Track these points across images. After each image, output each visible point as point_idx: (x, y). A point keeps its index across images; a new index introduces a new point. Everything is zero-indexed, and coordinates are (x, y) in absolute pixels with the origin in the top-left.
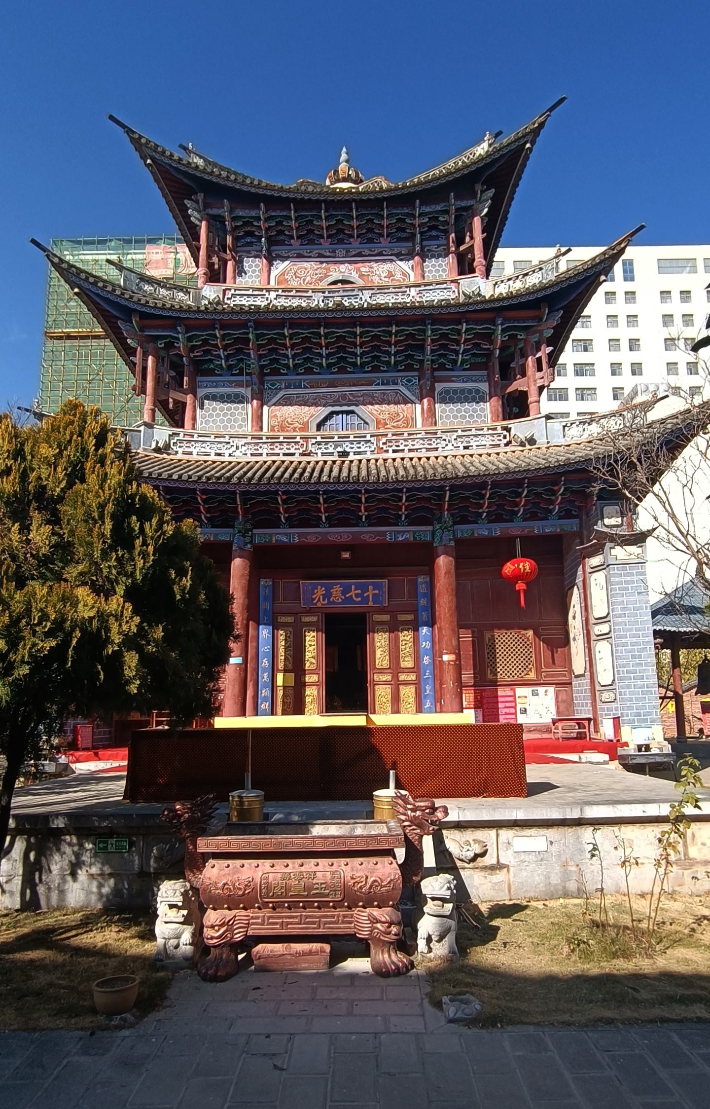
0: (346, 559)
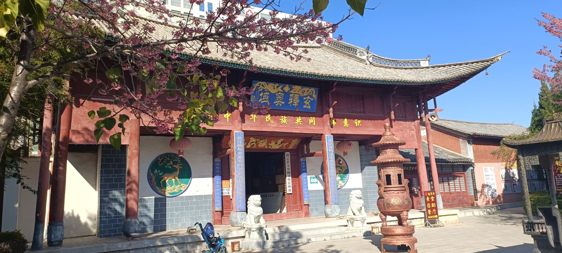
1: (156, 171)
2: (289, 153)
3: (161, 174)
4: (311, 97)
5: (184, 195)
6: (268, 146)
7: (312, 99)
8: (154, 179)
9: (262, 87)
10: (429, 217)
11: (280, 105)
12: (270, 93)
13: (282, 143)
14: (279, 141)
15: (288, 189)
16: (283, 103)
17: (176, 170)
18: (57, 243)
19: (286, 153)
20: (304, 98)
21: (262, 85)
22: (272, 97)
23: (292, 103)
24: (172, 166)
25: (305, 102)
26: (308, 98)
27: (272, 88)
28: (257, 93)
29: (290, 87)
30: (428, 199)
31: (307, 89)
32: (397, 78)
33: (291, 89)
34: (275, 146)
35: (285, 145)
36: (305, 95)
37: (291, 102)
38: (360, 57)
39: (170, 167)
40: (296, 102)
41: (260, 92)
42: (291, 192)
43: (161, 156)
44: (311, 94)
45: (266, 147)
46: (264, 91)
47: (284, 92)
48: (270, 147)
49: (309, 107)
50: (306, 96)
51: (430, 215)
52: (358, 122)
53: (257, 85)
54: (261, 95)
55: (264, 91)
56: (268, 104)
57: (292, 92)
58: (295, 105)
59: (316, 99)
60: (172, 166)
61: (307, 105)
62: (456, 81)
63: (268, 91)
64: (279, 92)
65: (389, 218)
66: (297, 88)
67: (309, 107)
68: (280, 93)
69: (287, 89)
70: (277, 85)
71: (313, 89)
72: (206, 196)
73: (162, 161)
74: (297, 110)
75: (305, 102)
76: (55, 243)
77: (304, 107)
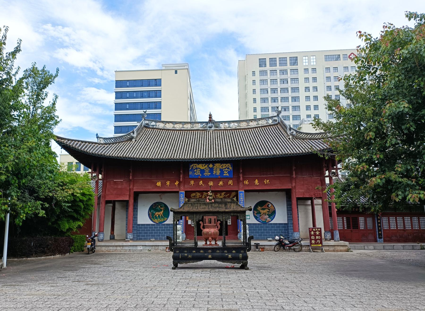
0: (178, 250)
1: (152, 211)
4: (228, 168)
8: (151, 215)
10: (312, 245)
13: (225, 194)
14: (223, 194)
16: (210, 174)
17: (161, 210)
22: (202, 171)
23: (216, 173)
25: (225, 172)
26: (226, 169)
27: (201, 166)
29: (213, 165)
30: (312, 233)
31: (225, 164)
33: (214, 166)
36: (224, 168)
40: (218, 172)
41: (195, 169)
43: (154, 204)
44: (228, 167)
46: (196, 169)
47: (209, 168)
49: (228, 175)
50: (225, 169)
51: (314, 244)
52: (267, 181)
53: (192, 165)
54: (195, 171)
55: (196, 169)
63: (199, 169)
66: (217, 165)
67: (228, 175)
69: (211, 166)
74: (219, 177)
75: (225, 172)
77: (224, 175)
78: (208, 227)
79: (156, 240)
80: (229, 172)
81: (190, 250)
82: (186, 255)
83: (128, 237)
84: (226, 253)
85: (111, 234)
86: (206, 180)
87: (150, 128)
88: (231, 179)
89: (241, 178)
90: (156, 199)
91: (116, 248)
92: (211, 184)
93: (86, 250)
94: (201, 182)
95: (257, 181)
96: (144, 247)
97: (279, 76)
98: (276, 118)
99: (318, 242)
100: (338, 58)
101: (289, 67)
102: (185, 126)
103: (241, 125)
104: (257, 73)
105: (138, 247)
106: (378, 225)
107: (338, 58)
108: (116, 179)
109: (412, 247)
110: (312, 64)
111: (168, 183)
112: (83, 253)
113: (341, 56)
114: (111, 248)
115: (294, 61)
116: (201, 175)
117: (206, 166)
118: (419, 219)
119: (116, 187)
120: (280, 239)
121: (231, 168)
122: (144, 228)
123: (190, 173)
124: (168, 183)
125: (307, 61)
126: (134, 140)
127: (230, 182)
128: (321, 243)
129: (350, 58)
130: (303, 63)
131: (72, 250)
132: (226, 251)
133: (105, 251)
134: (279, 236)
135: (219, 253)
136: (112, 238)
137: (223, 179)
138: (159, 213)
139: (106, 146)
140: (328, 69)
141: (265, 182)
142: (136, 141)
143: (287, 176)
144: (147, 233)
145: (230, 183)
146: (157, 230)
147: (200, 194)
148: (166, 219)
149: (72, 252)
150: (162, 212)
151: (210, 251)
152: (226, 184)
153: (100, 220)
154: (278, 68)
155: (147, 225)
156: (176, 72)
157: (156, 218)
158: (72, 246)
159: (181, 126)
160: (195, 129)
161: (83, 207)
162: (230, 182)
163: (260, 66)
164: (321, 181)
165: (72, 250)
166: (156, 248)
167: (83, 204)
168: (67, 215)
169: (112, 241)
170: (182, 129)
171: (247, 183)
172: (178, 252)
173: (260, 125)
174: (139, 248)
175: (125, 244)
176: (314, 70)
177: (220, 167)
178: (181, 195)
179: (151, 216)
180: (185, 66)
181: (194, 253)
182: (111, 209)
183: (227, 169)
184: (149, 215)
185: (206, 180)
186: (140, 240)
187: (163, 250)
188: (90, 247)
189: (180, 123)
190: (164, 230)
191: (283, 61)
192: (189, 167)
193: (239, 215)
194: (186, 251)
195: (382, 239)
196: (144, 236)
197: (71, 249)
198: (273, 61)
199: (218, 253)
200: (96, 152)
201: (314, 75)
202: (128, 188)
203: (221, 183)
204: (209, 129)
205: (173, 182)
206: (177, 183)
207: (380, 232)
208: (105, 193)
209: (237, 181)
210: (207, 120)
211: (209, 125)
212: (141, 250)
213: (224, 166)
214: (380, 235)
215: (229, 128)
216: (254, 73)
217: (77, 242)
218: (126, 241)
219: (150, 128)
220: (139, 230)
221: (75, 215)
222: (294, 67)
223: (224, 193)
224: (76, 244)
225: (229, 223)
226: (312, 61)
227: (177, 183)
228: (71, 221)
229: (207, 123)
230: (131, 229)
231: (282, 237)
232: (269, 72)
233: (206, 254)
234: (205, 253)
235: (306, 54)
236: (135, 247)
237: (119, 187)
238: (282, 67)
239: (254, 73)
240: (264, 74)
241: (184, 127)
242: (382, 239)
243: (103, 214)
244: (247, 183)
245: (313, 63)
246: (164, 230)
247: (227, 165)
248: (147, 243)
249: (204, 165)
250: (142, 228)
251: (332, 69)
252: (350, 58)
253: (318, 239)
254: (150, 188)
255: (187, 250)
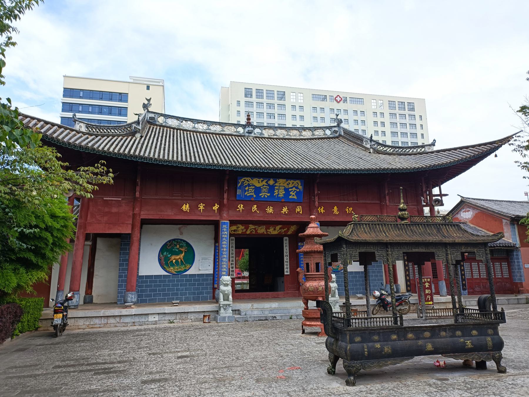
0: (358, 335)
1: (165, 253)
2: (287, 238)
3: (169, 256)
4: (297, 188)
5: (187, 273)
6: (267, 232)
7: (298, 190)
8: (163, 260)
9: (247, 182)
11: (266, 196)
12: (255, 186)
13: (280, 229)
14: (278, 228)
15: (285, 270)
16: (269, 194)
18: (73, 307)
19: (285, 238)
20: (290, 190)
21: (247, 180)
22: (258, 190)
23: (278, 195)
24: (178, 249)
25: (291, 193)
26: (294, 189)
27: (256, 182)
28: (243, 187)
31: (292, 181)
32: (385, 166)
33: (276, 182)
34: (273, 231)
35: (283, 230)
36: (290, 186)
37: (277, 193)
38: (366, 146)
39: (177, 250)
40: (282, 193)
41: (246, 186)
42: (289, 273)
43: (170, 241)
45: (265, 233)
47: (269, 185)
48: (269, 233)
49: (295, 197)
50: (292, 188)
53: (242, 180)
54: (247, 188)
55: (249, 185)
56: (255, 196)
57: (276, 184)
58: (281, 195)
59: (302, 190)
60: (178, 249)
61: (293, 196)
62: (463, 164)
63: (253, 185)
64: (264, 185)
65: (310, 302)
66: (281, 181)
67: (295, 197)
68: (265, 186)
69: (271, 182)
70: (262, 179)
71: (298, 181)
72: (207, 275)
73: (170, 245)
74: (283, 200)
75: (291, 193)
76: (71, 307)
77: (290, 197)
78: (313, 278)
79: (181, 303)
80: (297, 194)
81: (384, 333)
82: (378, 346)
83: (129, 299)
84: (459, 337)
85: (87, 293)
86: (262, 204)
87: (157, 125)
88: (298, 203)
89: (317, 203)
90: (171, 233)
91: (106, 320)
92: (270, 210)
93: (44, 326)
94: (255, 208)
95: (335, 208)
96: (162, 316)
97: (265, 110)
98: (336, 129)
99: (428, 298)
100: (325, 98)
101: (276, 101)
102: (211, 127)
103: (292, 134)
104: (243, 104)
105: (150, 317)
106: (461, 272)
107: (325, 98)
108: (109, 196)
109: (517, 300)
110: (299, 101)
111: (201, 207)
112: (36, 333)
113: (328, 97)
114: (97, 321)
115: (282, 95)
116: (255, 196)
117: (264, 183)
118: (501, 265)
119: (106, 210)
120: (382, 294)
121: (300, 187)
122: (150, 282)
123: (239, 192)
124: (201, 207)
125: (294, 97)
126: (138, 135)
127: (299, 209)
128: (432, 300)
129: (337, 101)
130: (291, 99)
131: (17, 331)
132: (458, 333)
133: (84, 327)
134: (380, 290)
135: (446, 337)
136: (88, 301)
137: (288, 204)
138: (178, 257)
139: (91, 138)
140: (315, 108)
141: (347, 210)
142: (142, 137)
143: (374, 203)
144: (155, 290)
145: (299, 210)
146: (173, 285)
147: (243, 228)
148: (188, 266)
149: (17, 335)
150: (182, 256)
151: (427, 334)
152: (292, 211)
153: (73, 269)
154: (265, 100)
155: (156, 276)
156: (148, 88)
157: (173, 265)
158: (19, 321)
159: (205, 127)
160: (227, 133)
161: (51, 241)
162: (299, 209)
163: (246, 96)
164: (418, 211)
165: (17, 331)
166: (184, 316)
167: (52, 235)
168: (13, 257)
169: (89, 307)
170: (208, 131)
171: (322, 211)
172: (358, 339)
173: (316, 137)
174: (151, 319)
175: (124, 312)
176: (301, 107)
177: (285, 185)
178: (224, 226)
179: (164, 262)
180: (159, 82)
181: (395, 340)
182: (88, 250)
183: (295, 188)
184: (160, 260)
185: (262, 204)
186: (152, 302)
187: (197, 320)
188: (59, 322)
189: (205, 122)
190: (186, 285)
191: (270, 94)
192: (236, 183)
193: (475, 250)
194: (376, 338)
195: (467, 291)
196: (150, 296)
197: (15, 329)
198: (260, 93)
199: (444, 337)
200: (77, 142)
201: (302, 114)
202: (131, 213)
203: (285, 210)
204: (247, 134)
205: (209, 206)
206: (216, 207)
207: (464, 282)
208: (86, 220)
209: (310, 208)
210: (243, 122)
211: (247, 129)
212: (155, 323)
213: (292, 183)
214: (464, 285)
215: (275, 137)
216: (239, 102)
217: (28, 312)
218: (126, 307)
219: (157, 125)
220: (142, 286)
221: (33, 258)
222: (281, 102)
223: (280, 226)
224: (25, 318)
225: (287, 272)
226: (299, 98)
227: (216, 207)
228: (22, 270)
229: (244, 127)
230: (135, 285)
231: (383, 292)
232: (255, 104)
233: (420, 342)
234: (418, 338)
235: (295, 90)
236: (144, 317)
237: (114, 210)
238: (269, 100)
239: (239, 102)
240: (250, 105)
241: (210, 129)
242: (467, 291)
243: (80, 259)
244: (322, 211)
245: (301, 102)
246: (186, 285)
247: (295, 182)
248: (168, 309)
249: (260, 180)
250: (146, 282)
251: (298, 117)
252: (337, 101)
253: (428, 294)
254: (170, 214)
255: (379, 334)
